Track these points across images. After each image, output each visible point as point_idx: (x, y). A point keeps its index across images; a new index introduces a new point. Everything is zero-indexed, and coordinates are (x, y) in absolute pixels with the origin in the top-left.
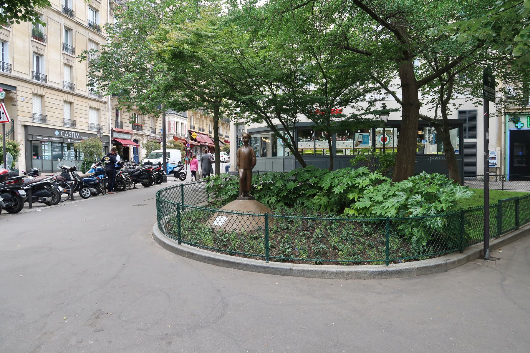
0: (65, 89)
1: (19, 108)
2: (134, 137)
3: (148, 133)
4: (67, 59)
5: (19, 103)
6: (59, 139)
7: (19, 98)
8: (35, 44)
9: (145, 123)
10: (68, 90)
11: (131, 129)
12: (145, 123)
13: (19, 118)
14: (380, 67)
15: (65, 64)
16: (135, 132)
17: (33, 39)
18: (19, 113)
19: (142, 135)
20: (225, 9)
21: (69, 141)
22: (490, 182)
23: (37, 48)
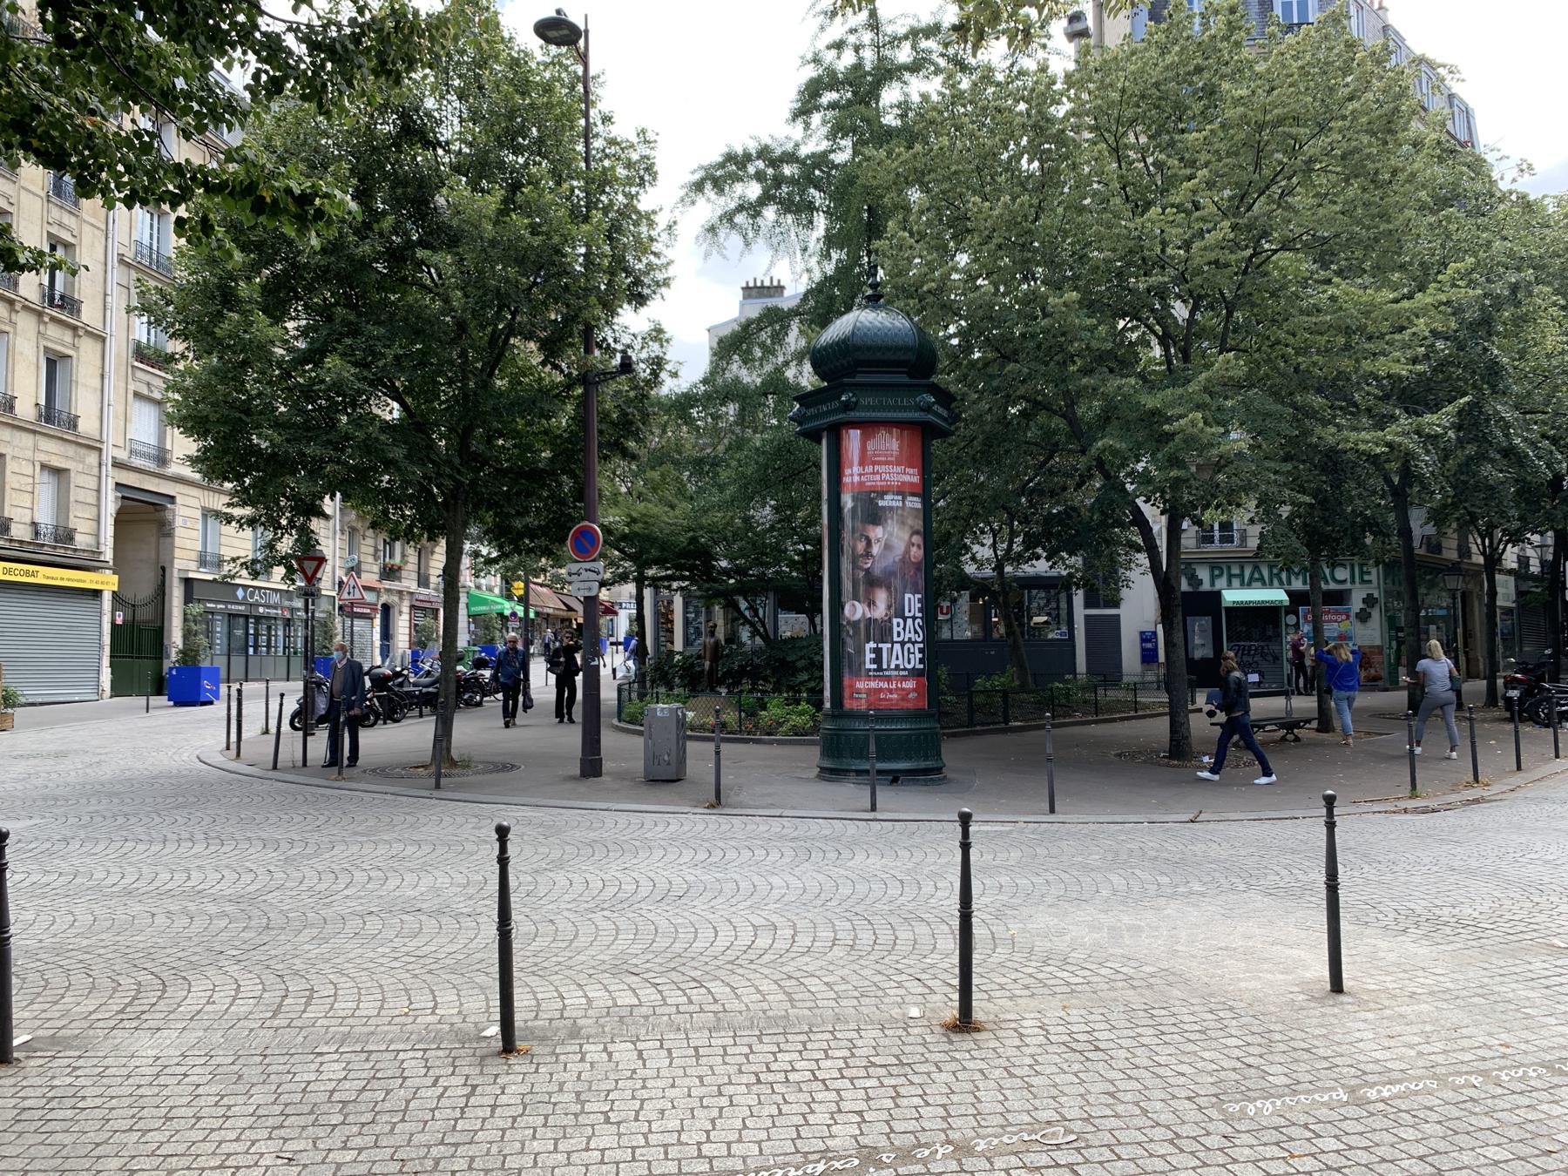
0: (138, 462)
1: (178, 542)
2: (384, 599)
3: (413, 586)
4: (148, 384)
5: (179, 532)
6: (243, 608)
7: (178, 522)
8: (139, 374)
9: (407, 562)
10: (151, 466)
11: (377, 577)
12: (407, 562)
13: (178, 564)
14: (963, 534)
15: (137, 395)
16: (387, 584)
17: (136, 364)
18: (177, 553)
19: (400, 592)
20: (347, 11)
21: (261, 610)
22: (915, 662)
23: (148, 384)
